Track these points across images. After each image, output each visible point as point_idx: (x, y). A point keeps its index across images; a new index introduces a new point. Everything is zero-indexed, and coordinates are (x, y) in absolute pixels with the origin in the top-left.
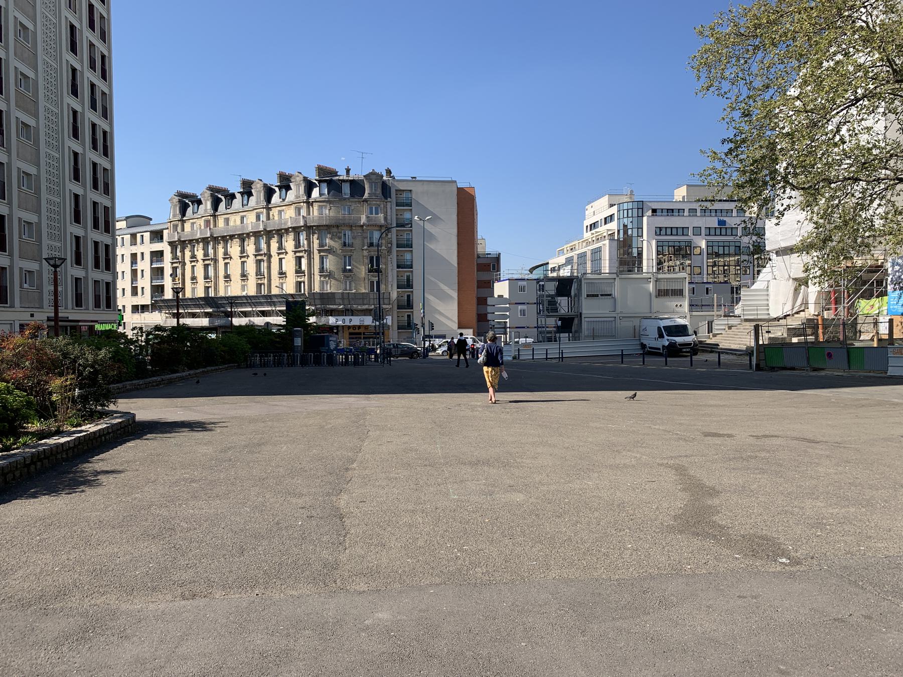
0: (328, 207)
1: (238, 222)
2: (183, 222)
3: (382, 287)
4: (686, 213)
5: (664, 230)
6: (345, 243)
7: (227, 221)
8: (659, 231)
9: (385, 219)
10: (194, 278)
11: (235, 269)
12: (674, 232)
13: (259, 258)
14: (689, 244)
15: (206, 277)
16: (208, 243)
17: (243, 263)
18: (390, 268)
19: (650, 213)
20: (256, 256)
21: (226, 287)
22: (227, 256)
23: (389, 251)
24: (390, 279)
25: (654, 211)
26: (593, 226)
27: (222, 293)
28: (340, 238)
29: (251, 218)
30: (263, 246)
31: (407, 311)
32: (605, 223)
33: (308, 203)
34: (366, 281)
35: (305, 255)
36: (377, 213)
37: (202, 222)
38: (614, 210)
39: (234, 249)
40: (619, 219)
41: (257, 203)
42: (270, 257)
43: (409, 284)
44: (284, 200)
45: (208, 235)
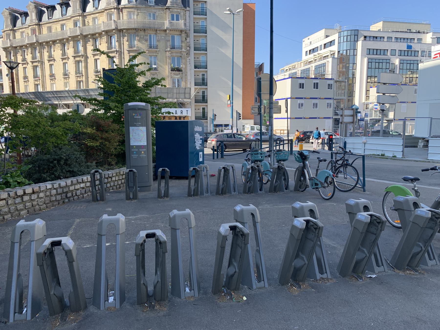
0: (136, 13)
1: (59, 29)
2: (14, 31)
3: (183, 84)
4: (386, 40)
5: (375, 51)
6: (151, 45)
7: (50, 29)
8: (370, 51)
9: (185, 24)
10: (25, 77)
11: (58, 69)
12: (378, 53)
13: (78, 59)
14: (388, 61)
15: (35, 76)
16: (35, 48)
17: (65, 64)
18: (188, 68)
19: (362, 38)
20: (75, 57)
21: (52, 85)
22: (51, 59)
23: (188, 54)
24: (189, 78)
25: (365, 37)
26: (312, 51)
27: (48, 89)
28: (146, 40)
29: (70, 25)
30: (81, 48)
31: (201, 106)
32: (325, 48)
33: (118, 9)
34: (170, 78)
35: (117, 55)
36: (178, 20)
37: (29, 31)
38: (335, 37)
39: (57, 52)
40: (339, 43)
41: (74, 11)
42: (87, 58)
43: (203, 82)
44: (97, 9)
45: (35, 41)
